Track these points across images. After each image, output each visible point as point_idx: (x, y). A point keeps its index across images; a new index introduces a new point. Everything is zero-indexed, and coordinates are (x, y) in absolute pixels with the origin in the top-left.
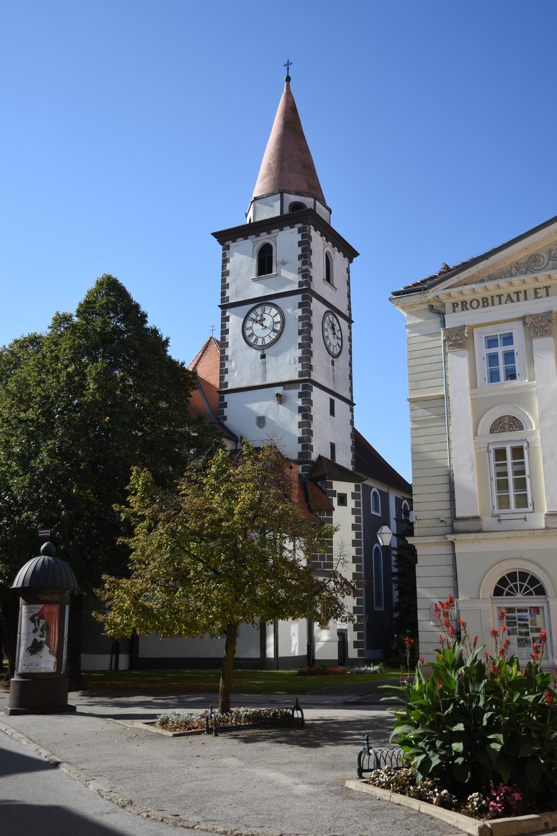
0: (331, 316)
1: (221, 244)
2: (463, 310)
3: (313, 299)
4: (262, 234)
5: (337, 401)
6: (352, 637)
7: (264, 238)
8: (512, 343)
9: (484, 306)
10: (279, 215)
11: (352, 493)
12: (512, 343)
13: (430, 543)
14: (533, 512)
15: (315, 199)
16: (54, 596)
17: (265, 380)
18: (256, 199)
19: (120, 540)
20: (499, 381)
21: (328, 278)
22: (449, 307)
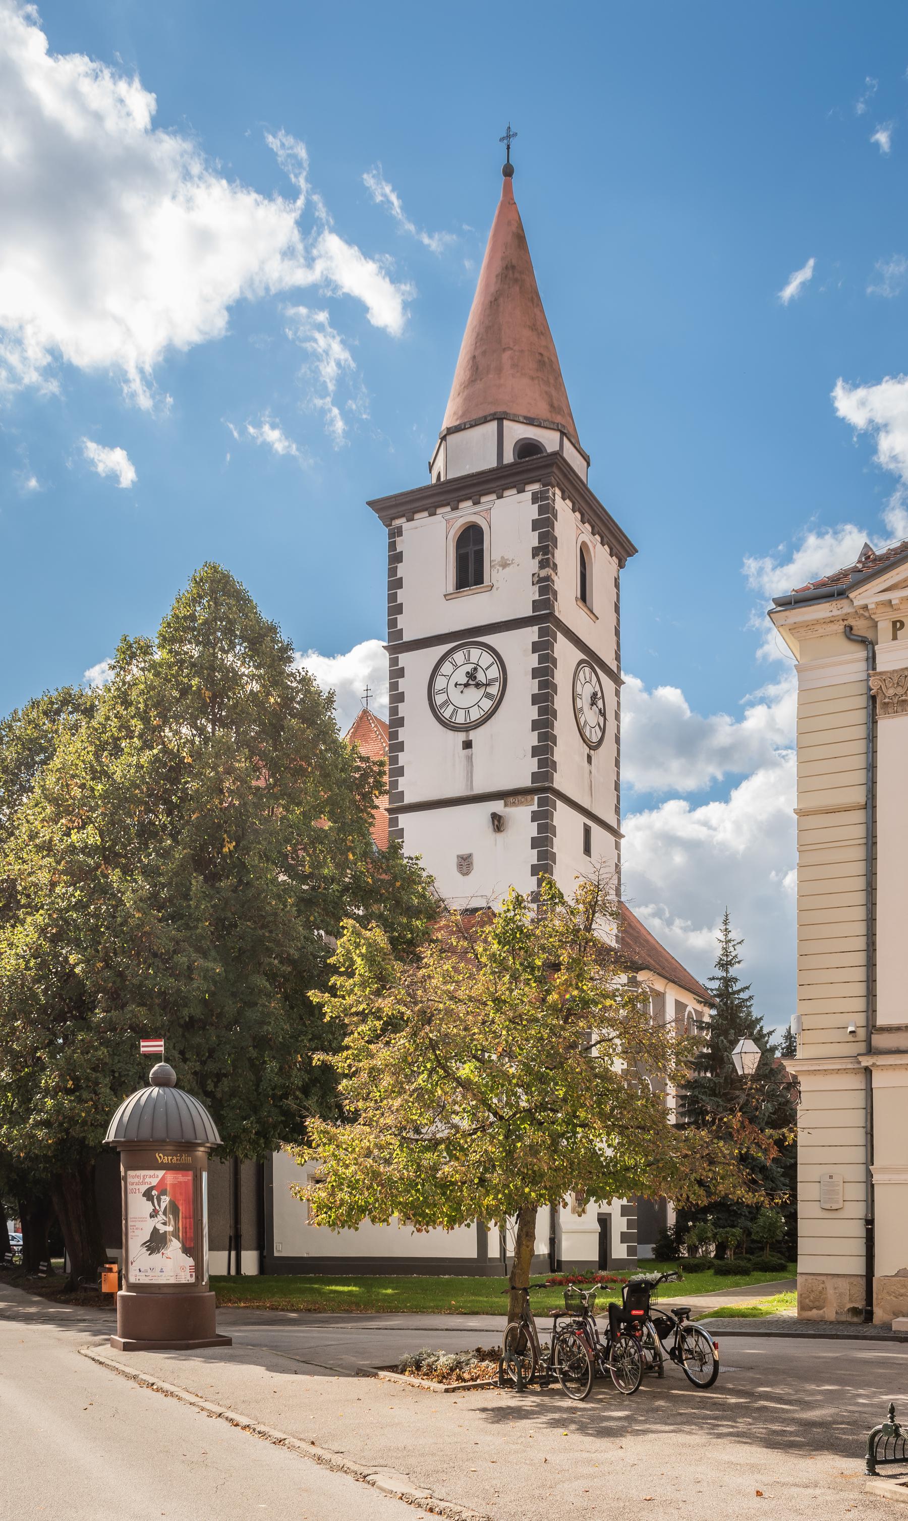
0: (587, 669)
1: (387, 526)
3: (559, 634)
4: (462, 505)
5: (595, 829)
6: (619, 1225)
7: (467, 513)
10: (494, 464)
13: (825, 1070)
15: (563, 434)
16: (181, 1156)
18: (451, 431)
19: (318, 1058)
22: (885, 627)
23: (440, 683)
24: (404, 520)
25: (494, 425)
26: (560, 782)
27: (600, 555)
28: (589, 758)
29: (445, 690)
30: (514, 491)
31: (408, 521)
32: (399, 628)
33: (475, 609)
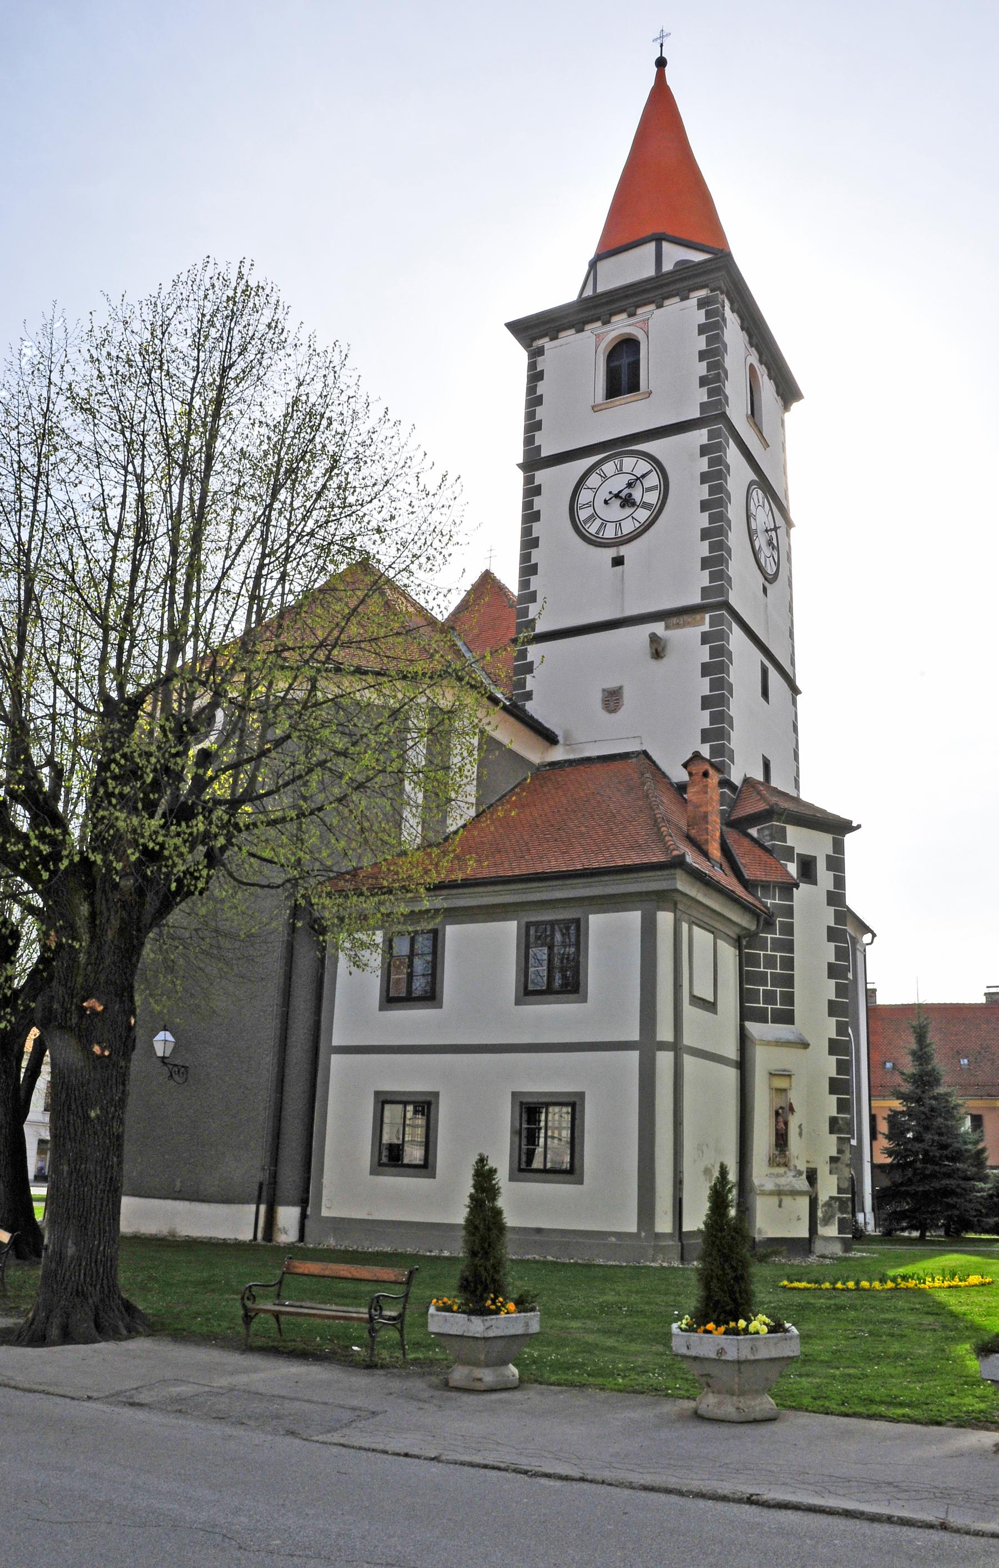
7: (621, 325)
8: (814, 859)
11: (828, 856)
12: (814, 859)
17: (623, 610)
20: (638, 390)
23: (585, 496)
24: (547, 339)
25: (652, 246)
27: (767, 388)
29: (591, 504)
31: (551, 340)
33: (630, 416)
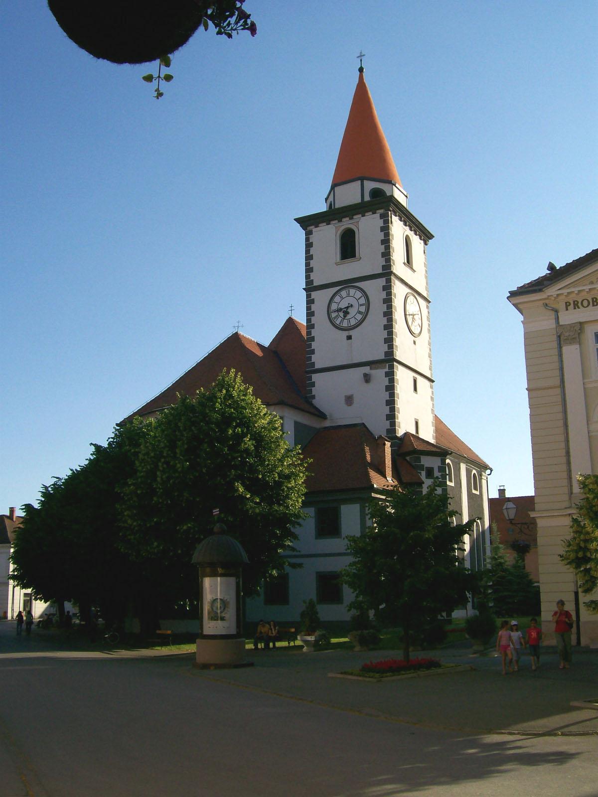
2: (575, 308)
4: (344, 220)
7: (346, 223)
9: (593, 305)
14: (491, 471)
20: (355, 257)
21: (409, 262)
22: (561, 306)
25: (359, 182)
26: (399, 355)
28: (415, 343)
30: (371, 213)
31: (316, 227)
32: (310, 241)
33: (350, 270)
